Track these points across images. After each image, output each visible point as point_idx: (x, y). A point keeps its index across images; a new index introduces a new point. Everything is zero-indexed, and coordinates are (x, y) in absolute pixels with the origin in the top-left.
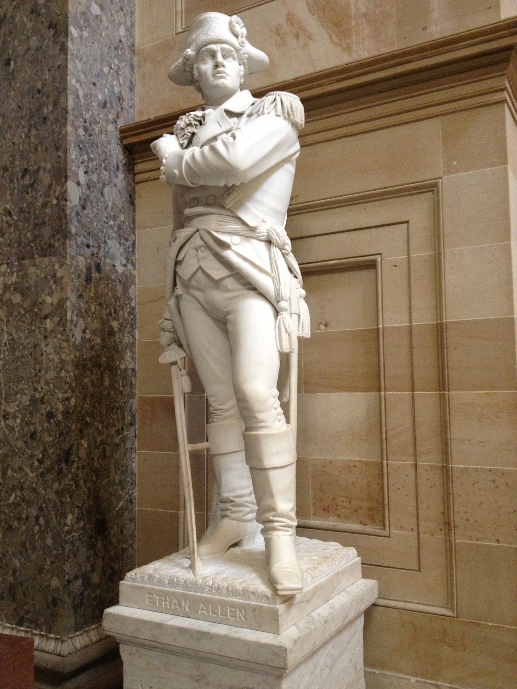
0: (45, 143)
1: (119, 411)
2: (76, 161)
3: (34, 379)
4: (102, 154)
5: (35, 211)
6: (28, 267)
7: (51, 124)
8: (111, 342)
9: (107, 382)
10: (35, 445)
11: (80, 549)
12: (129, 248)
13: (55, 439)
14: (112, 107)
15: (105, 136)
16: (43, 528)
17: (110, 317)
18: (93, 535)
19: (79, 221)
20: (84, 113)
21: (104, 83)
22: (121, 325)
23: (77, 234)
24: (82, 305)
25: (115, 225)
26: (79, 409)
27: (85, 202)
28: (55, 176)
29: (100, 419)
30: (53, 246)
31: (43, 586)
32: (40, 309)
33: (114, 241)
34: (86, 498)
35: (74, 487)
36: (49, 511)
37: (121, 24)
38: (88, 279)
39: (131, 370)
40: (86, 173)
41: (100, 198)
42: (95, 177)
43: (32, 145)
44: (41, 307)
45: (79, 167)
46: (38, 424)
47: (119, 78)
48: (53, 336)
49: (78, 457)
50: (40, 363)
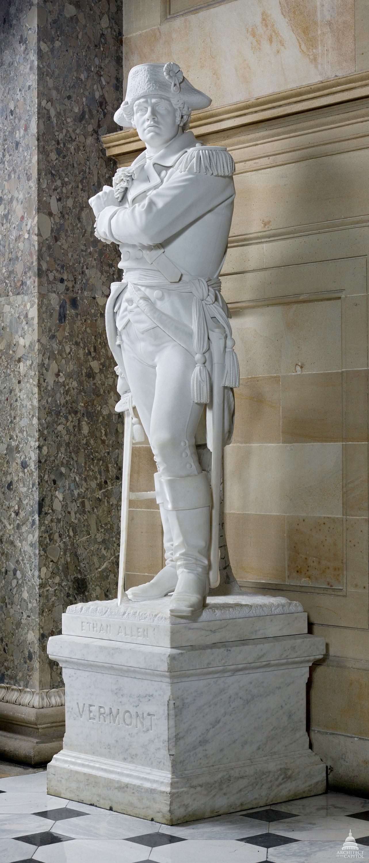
0: (17, 171)
1: (101, 462)
2: (47, 190)
3: (10, 426)
4: (79, 174)
5: (9, 245)
6: (4, 305)
7: (23, 151)
8: (90, 386)
9: (85, 430)
10: (12, 496)
11: (55, 605)
12: (113, 274)
13: (29, 489)
14: (92, 116)
15: (83, 152)
16: (20, 582)
17: (89, 357)
18: (71, 593)
19: (50, 256)
20: (57, 133)
21: (82, 91)
22: (103, 365)
23: (48, 270)
24: (55, 346)
25: (96, 251)
26: (52, 458)
27: (58, 233)
28: (26, 208)
29: (77, 470)
30: (26, 283)
31: (20, 641)
32: (14, 352)
33: (94, 270)
34: (62, 553)
35: (48, 540)
36: (25, 564)
37: (103, 14)
38: (62, 317)
39: (117, 417)
40: (59, 200)
41: (77, 225)
42: (70, 203)
43: (6, 172)
44: (15, 349)
45: (51, 196)
46: (14, 474)
47: (100, 80)
48: (26, 380)
49: (53, 510)
50: (14, 409)
